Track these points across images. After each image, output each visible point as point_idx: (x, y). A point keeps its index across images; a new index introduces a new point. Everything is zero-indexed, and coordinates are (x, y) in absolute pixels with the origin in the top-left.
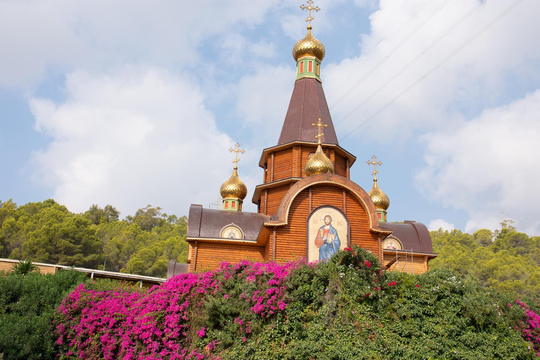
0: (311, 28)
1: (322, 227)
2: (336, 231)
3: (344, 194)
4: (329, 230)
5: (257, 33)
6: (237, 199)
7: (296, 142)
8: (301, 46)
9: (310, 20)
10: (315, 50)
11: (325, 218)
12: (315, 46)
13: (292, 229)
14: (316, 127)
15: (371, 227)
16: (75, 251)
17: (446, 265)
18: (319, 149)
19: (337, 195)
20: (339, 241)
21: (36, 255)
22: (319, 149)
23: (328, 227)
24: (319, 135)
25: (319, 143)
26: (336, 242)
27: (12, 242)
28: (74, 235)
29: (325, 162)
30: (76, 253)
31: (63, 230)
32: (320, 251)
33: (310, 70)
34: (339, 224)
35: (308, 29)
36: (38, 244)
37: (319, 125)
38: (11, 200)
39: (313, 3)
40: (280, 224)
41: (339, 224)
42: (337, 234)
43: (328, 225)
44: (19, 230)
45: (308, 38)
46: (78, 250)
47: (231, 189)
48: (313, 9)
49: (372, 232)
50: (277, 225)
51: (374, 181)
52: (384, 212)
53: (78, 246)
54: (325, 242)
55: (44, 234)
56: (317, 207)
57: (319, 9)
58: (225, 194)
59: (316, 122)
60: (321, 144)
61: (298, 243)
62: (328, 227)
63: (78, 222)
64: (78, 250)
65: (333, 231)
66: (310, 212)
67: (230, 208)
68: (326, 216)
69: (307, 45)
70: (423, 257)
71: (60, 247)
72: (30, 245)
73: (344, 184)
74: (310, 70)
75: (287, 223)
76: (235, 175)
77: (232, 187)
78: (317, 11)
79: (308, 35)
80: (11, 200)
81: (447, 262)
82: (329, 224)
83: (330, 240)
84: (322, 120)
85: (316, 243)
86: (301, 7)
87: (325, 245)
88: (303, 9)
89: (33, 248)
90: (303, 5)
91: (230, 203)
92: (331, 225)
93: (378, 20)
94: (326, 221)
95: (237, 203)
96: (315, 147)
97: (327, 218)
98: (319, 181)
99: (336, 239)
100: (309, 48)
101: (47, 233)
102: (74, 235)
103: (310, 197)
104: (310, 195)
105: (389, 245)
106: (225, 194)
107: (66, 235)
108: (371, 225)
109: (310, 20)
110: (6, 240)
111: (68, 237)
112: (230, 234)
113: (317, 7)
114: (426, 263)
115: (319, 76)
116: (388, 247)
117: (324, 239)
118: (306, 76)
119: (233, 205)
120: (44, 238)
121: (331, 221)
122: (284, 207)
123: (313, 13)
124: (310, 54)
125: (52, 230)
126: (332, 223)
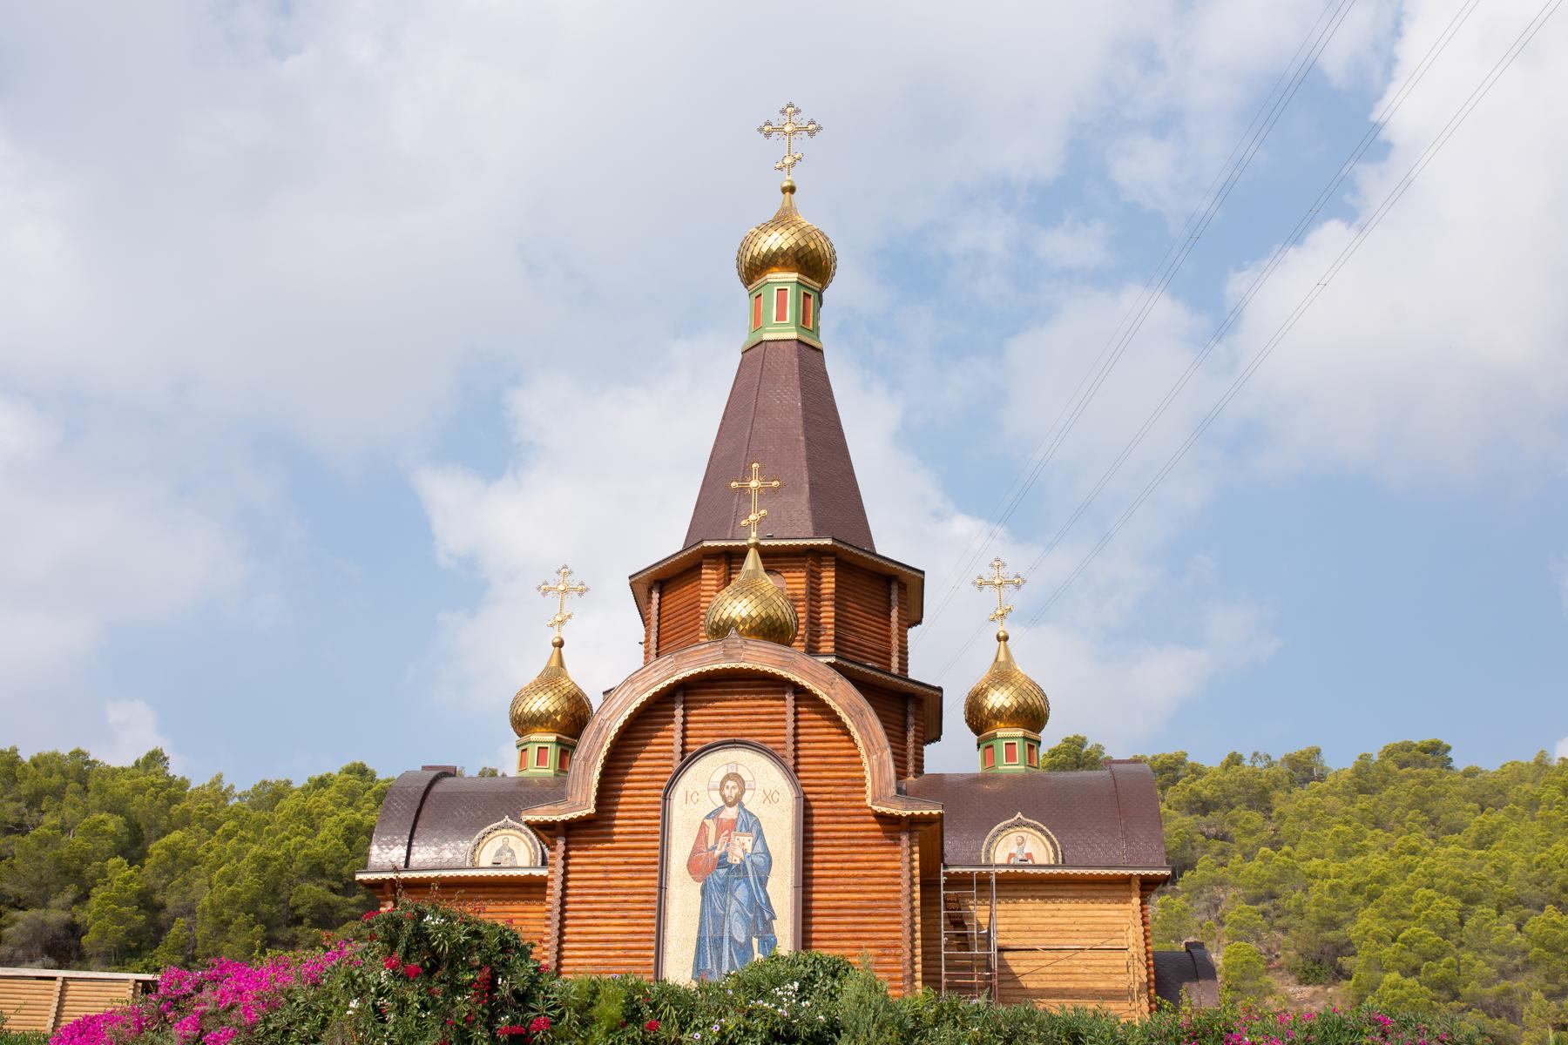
0: (792, 190)
1: (713, 815)
2: (757, 822)
3: (790, 698)
4: (734, 823)
5: (1053, 201)
6: (553, 738)
7: (706, 544)
8: (760, 243)
9: (793, 164)
10: (796, 253)
11: (722, 784)
12: (792, 242)
13: (621, 826)
14: (743, 492)
15: (869, 802)
16: (343, 914)
17: (1532, 875)
18: (752, 561)
19: (768, 704)
20: (767, 853)
21: (230, 935)
22: (752, 561)
23: (731, 813)
24: (752, 517)
25: (751, 541)
26: (755, 859)
27: (172, 901)
28: (338, 867)
29: (764, 600)
30: (345, 920)
31: (306, 856)
32: (703, 892)
33: (781, 316)
34: (769, 798)
35: (784, 190)
36: (233, 901)
37: (754, 484)
38: (219, 778)
39: (797, 111)
40: (571, 815)
41: (769, 798)
42: (760, 834)
43: (731, 805)
44: (195, 864)
45: (782, 220)
46: (352, 909)
47: (542, 709)
48: (799, 129)
49: (881, 817)
50: (563, 817)
51: (999, 639)
52: (1025, 738)
53: (352, 900)
54: (722, 862)
55: (252, 871)
56: (699, 747)
57: (819, 129)
58: (524, 724)
59: (746, 474)
60: (757, 546)
61: (639, 869)
62: (731, 813)
63: (349, 829)
64: (352, 909)
65: (751, 825)
66: (677, 764)
67: (534, 770)
68: (728, 777)
69: (777, 241)
70: (1127, 880)
71: (297, 907)
72: (212, 906)
73: (781, 667)
74: (781, 316)
75: (592, 810)
76: (554, 664)
77: (541, 704)
78: (812, 133)
79: (784, 210)
80: (219, 778)
81: (1538, 865)
82: (737, 801)
83: (739, 852)
84: (760, 470)
85: (693, 867)
86: (761, 130)
87: (722, 872)
88: (768, 135)
89: (221, 914)
90: (812, 122)
91: (533, 751)
92: (741, 806)
93: (1406, 109)
94: (727, 792)
95: (553, 753)
96: (741, 554)
97: (730, 783)
98: (701, 665)
99: (759, 848)
100: (774, 248)
101: (263, 867)
102: (338, 867)
103: (679, 719)
104: (679, 712)
105: (1014, 850)
106: (524, 724)
107: (317, 870)
108: (869, 793)
109: (793, 164)
110: (158, 897)
111: (323, 875)
112: (499, 853)
113: (812, 122)
114: (1136, 901)
115: (815, 331)
116: (1011, 855)
117: (717, 853)
118: (766, 337)
119: (541, 760)
120: (248, 882)
121: (743, 792)
122: (586, 759)
123: (802, 143)
124: (786, 267)
125: (276, 859)
126: (745, 799)
